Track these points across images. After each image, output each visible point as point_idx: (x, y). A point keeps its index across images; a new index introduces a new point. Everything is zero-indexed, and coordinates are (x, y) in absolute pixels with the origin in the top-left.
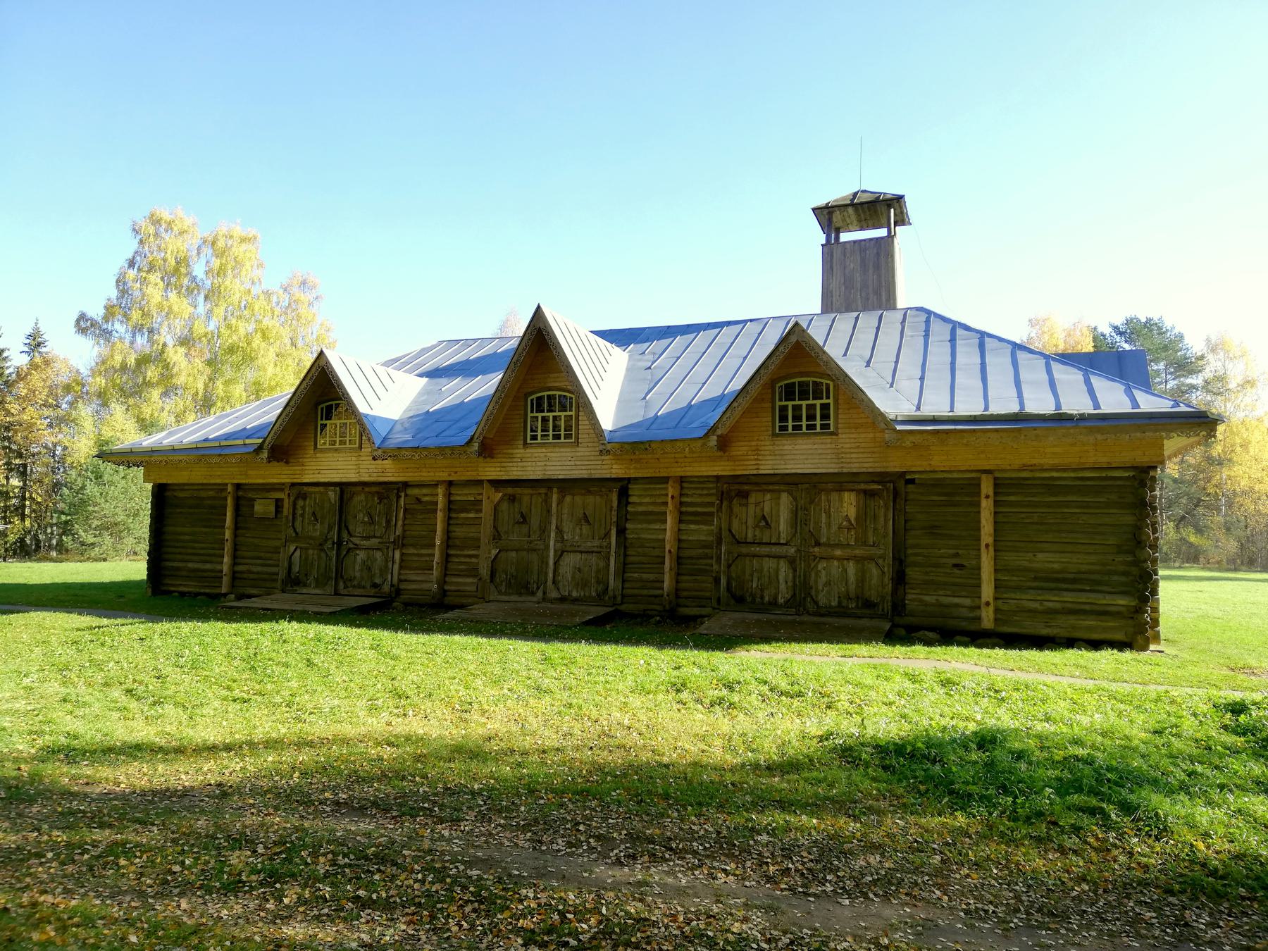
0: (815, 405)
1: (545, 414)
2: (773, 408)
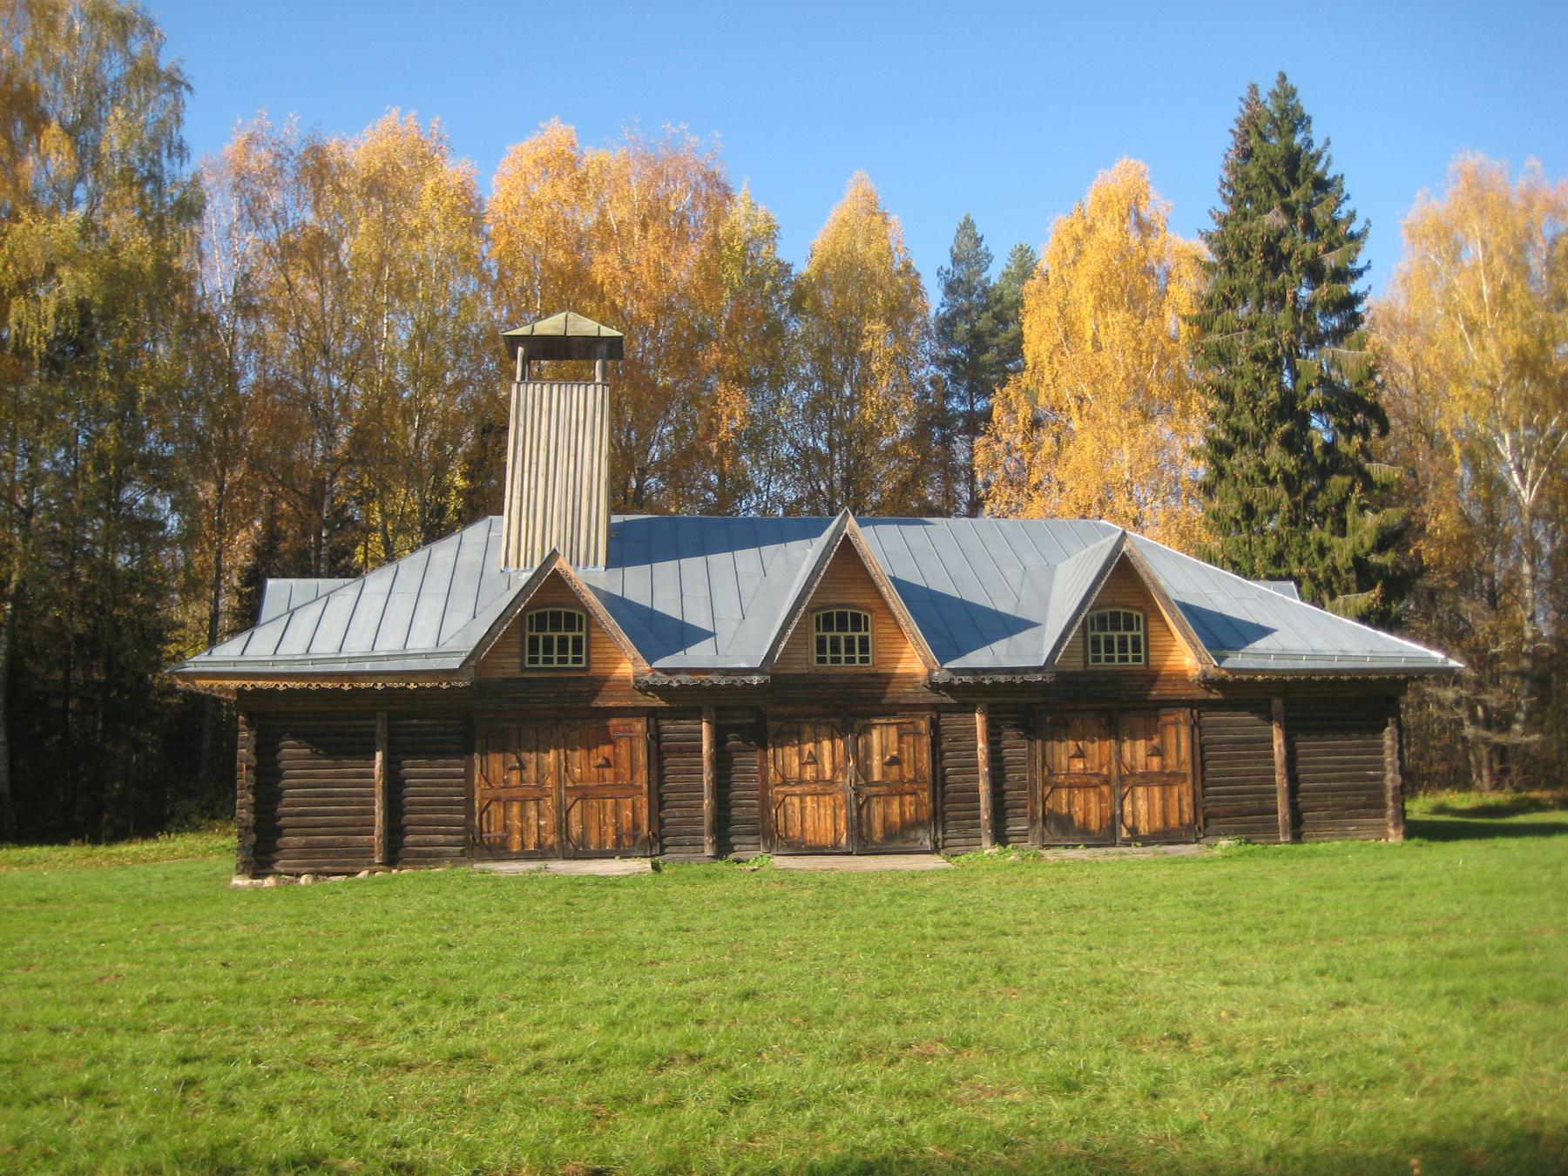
0: (838, 638)
1: (1109, 633)
2: (523, 637)
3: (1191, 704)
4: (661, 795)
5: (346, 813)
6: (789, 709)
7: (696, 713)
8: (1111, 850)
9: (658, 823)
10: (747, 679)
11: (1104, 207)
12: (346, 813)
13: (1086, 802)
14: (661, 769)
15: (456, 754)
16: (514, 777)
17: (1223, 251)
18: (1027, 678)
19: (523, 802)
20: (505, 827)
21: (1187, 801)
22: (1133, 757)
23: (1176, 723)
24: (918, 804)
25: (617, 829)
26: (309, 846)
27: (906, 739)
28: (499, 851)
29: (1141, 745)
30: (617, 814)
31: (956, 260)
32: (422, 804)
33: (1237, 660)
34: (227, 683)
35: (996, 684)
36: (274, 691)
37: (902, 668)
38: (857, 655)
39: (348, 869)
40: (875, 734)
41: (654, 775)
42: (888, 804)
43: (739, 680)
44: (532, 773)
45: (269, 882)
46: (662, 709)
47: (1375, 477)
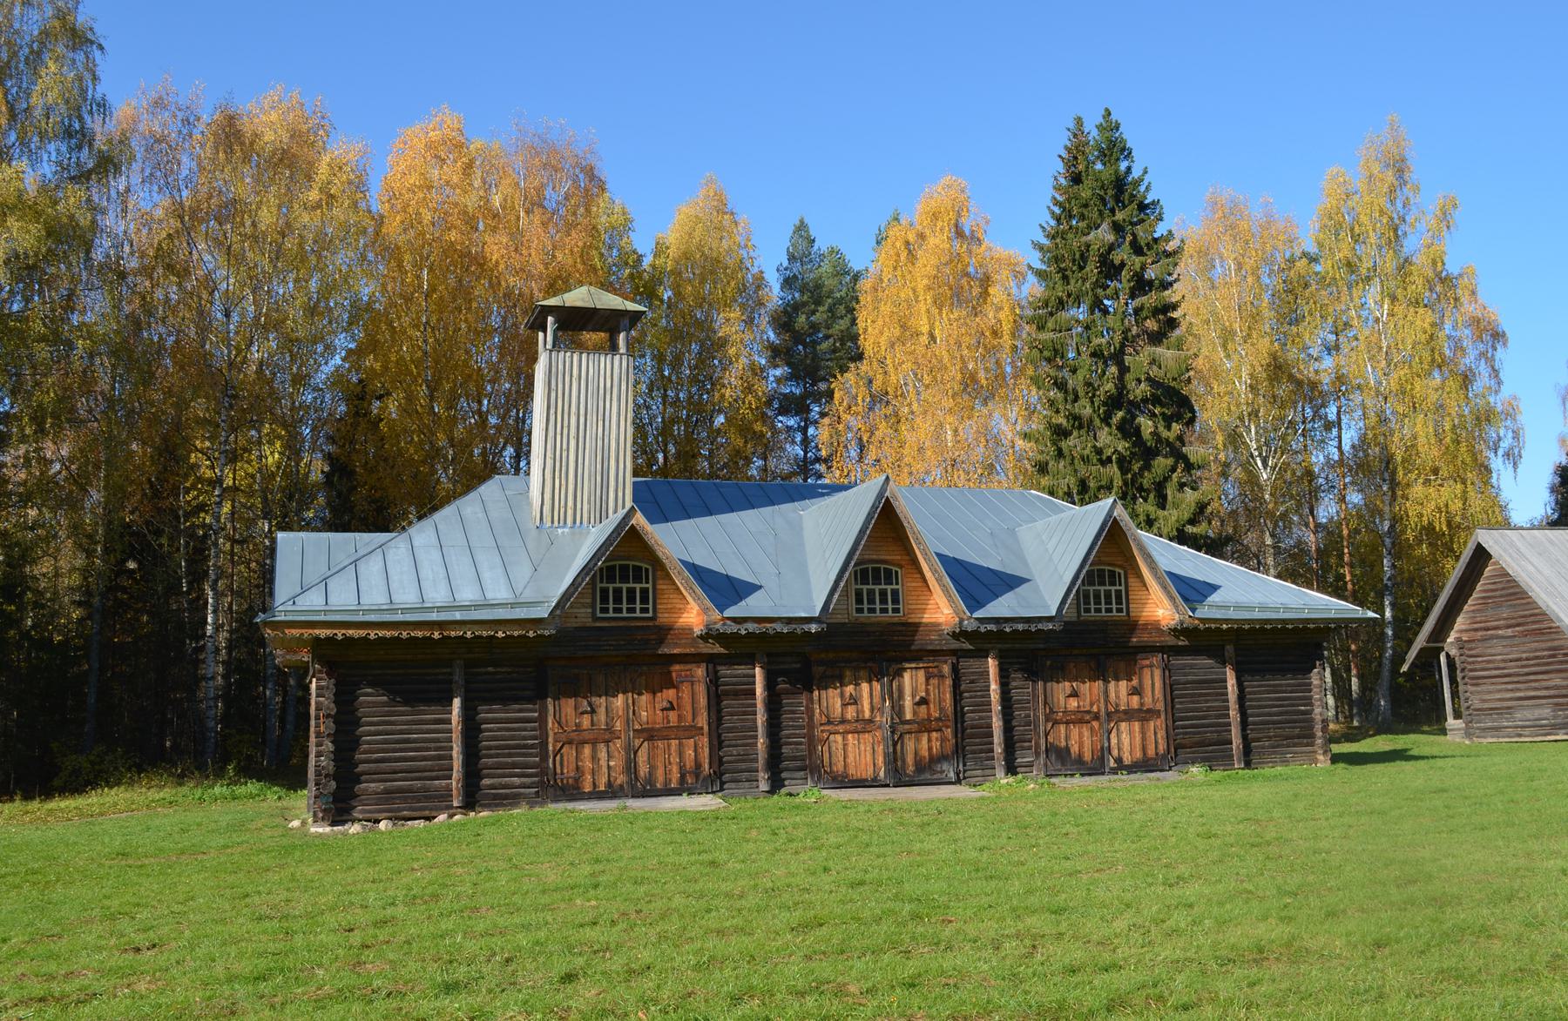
3: (1162, 649)
4: (719, 736)
5: (425, 759)
6: (831, 655)
7: (750, 660)
8: (1101, 778)
9: (717, 761)
10: (806, 627)
11: (935, 216)
12: (425, 759)
13: (1081, 735)
14: (719, 711)
15: (530, 700)
16: (586, 721)
17: (1057, 259)
18: (1040, 626)
19: (594, 743)
20: (578, 768)
21: (1161, 734)
22: (1117, 697)
23: (1151, 666)
24: (943, 740)
25: (681, 767)
26: (387, 791)
27: (932, 681)
28: (571, 791)
29: (1123, 684)
30: (681, 754)
31: (792, 258)
32: (497, 748)
33: (1204, 612)
34: (317, 632)
35: (1015, 631)
36: (365, 639)
37: (927, 618)
38: (890, 606)
39: (427, 813)
40: (907, 676)
41: (714, 717)
42: (918, 740)
43: (799, 628)
44: (601, 716)
45: (355, 829)
46: (719, 655)
47: (1192, 459)
